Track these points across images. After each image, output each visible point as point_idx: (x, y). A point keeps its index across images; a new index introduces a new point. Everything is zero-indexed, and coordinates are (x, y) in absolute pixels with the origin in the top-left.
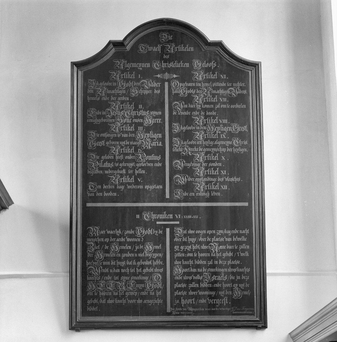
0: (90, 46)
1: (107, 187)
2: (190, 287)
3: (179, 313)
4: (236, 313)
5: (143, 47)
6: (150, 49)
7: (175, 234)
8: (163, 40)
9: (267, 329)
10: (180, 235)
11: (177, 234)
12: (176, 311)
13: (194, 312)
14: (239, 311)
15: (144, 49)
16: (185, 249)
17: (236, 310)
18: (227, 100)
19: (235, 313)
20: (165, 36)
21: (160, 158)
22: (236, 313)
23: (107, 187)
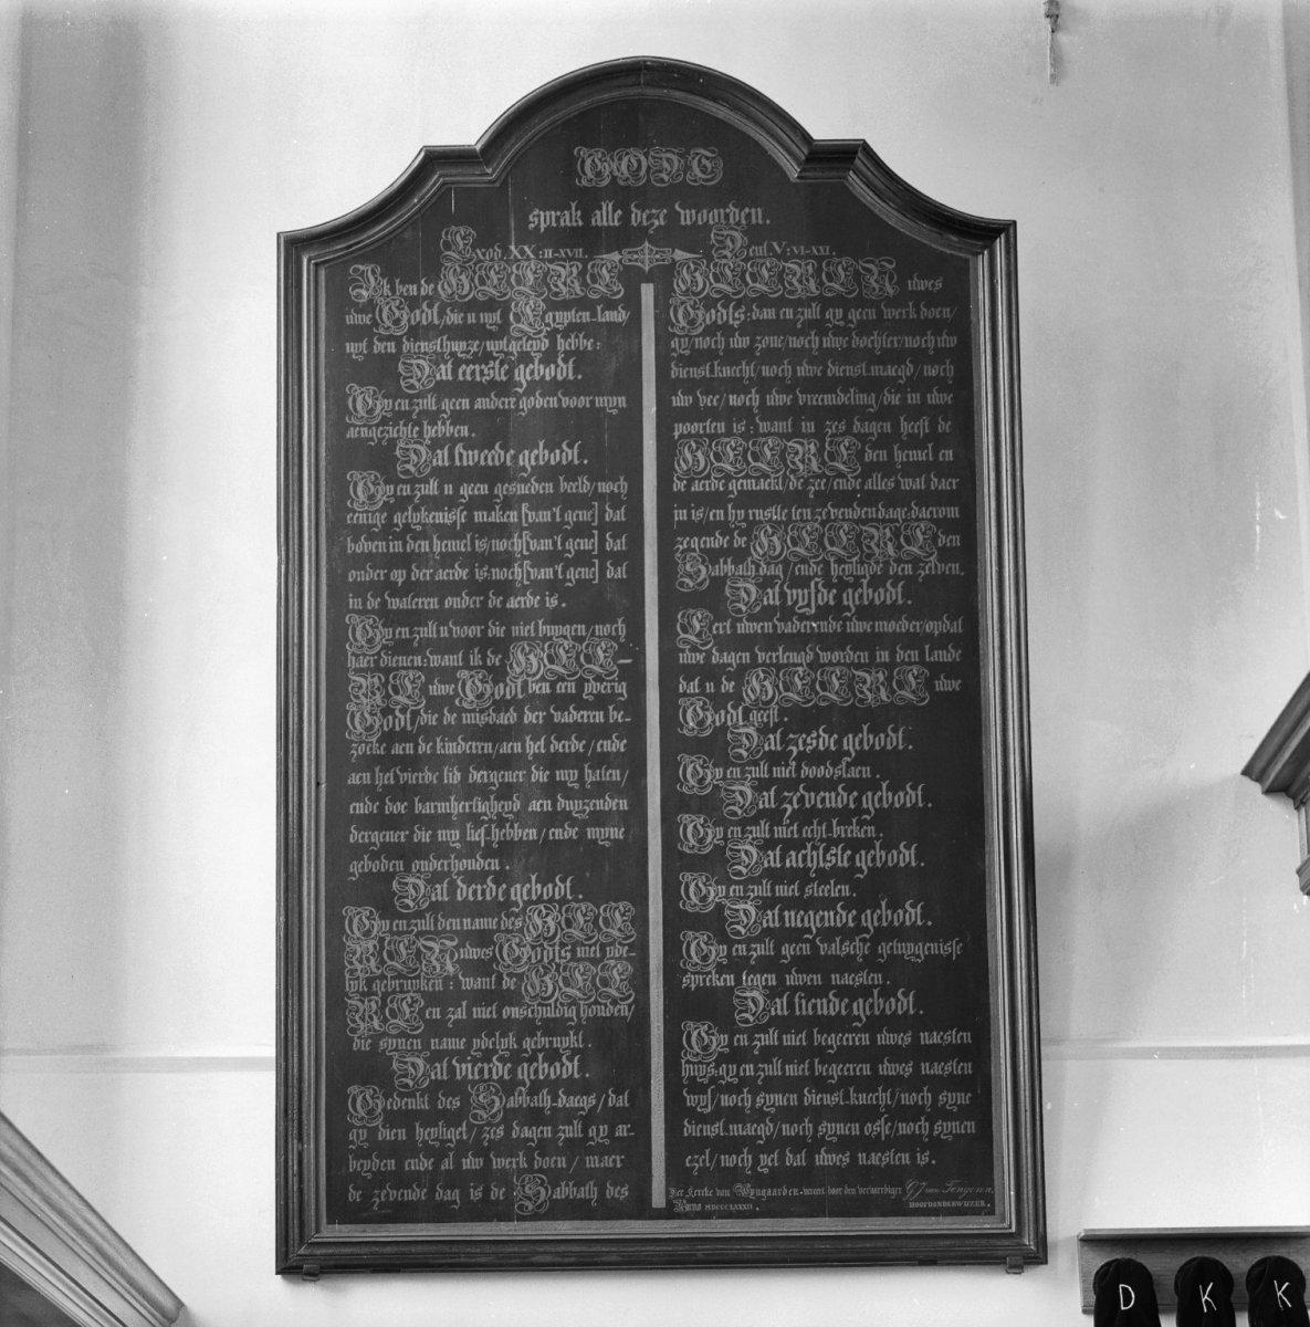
0: (351, 177)
1: (442, 865)
2: (755, 955)
3: (698, 1207)
4: (923, 1205)
5: (704, 161)
6: (822, 1010)
7: (733, 748)
8: (408, 902)
9: (1044, 1266)
10: (749, 930)
11: (731, 807)
12: (690, 1201)
13: (757, 1201)
14: (936, 1198)
15: (709, 170)
16: (760, 1076)
17: (922, 1194)
18: (764, 218)
19: (917, 1205)
20: (415, 887)
21: (684, 980)
22: (923, 1205)
23: (442, 865)
